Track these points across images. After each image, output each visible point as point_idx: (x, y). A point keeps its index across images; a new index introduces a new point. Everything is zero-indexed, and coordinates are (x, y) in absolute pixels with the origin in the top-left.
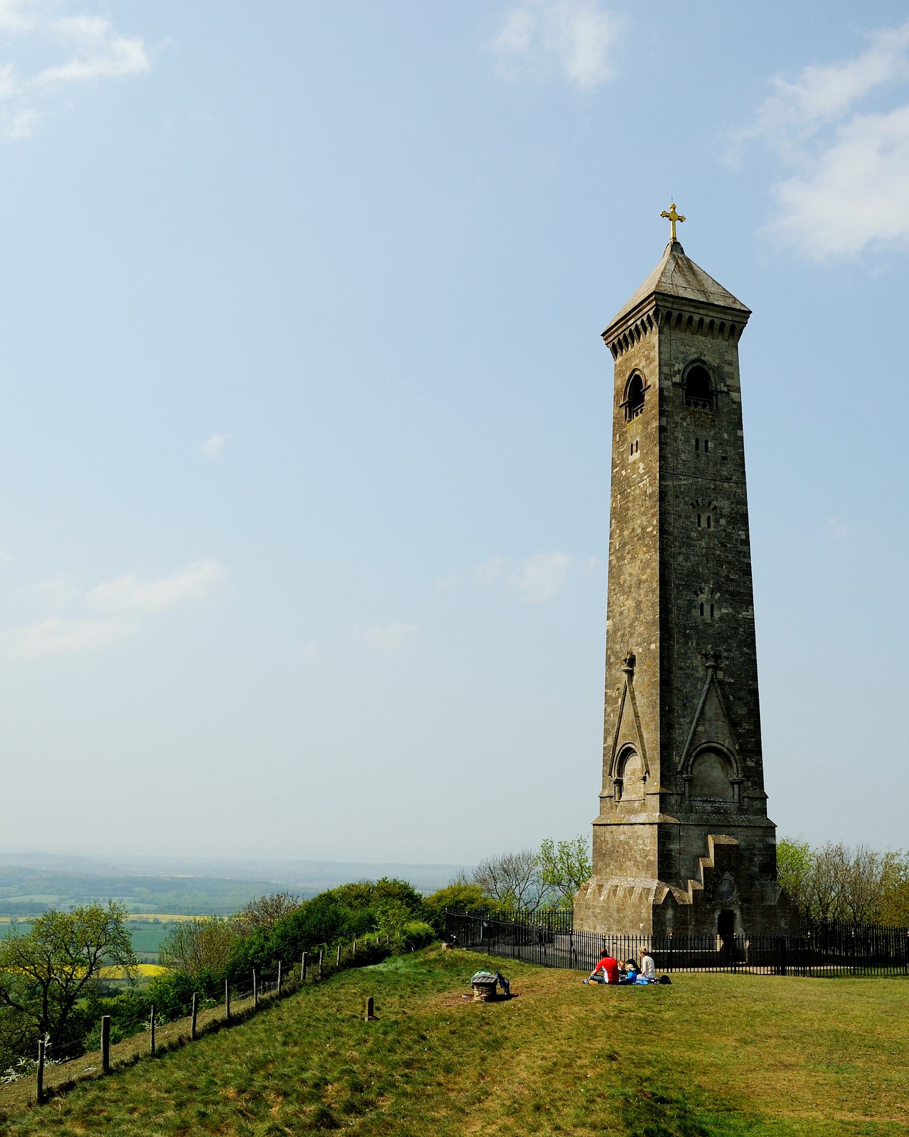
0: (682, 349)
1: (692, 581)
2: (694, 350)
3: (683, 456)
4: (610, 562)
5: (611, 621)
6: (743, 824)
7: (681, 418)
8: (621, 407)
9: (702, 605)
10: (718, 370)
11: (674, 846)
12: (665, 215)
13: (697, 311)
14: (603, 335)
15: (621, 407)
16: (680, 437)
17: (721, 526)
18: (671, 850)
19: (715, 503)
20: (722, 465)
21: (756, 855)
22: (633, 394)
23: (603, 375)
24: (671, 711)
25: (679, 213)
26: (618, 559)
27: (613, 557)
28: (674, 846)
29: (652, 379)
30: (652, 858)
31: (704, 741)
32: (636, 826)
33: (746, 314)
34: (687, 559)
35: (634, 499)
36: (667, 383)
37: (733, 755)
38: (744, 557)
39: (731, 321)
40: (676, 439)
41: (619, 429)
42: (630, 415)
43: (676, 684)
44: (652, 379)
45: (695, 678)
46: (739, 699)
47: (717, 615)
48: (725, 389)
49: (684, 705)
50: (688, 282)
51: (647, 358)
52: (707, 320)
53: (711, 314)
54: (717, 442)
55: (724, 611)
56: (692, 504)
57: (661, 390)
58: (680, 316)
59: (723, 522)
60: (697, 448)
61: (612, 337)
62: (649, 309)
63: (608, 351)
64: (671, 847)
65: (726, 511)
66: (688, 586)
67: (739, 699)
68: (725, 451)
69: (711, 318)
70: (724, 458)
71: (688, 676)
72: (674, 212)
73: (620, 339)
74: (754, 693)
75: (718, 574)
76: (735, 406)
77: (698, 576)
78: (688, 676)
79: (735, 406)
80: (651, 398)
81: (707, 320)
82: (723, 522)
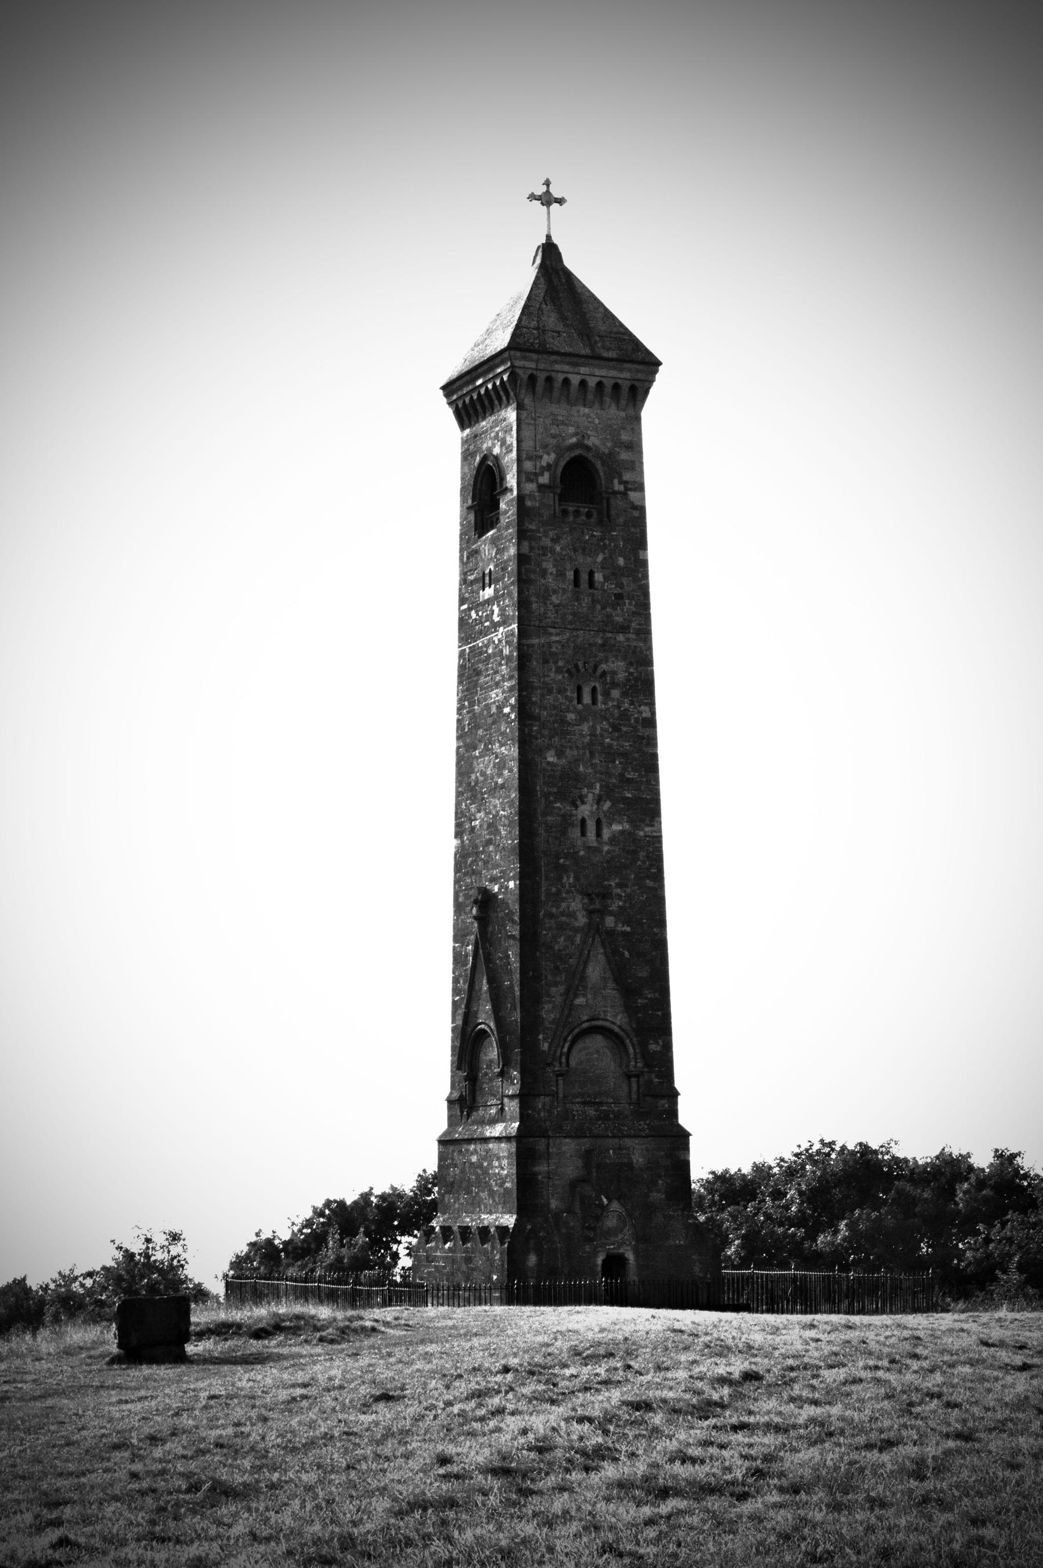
1: (568, 787)
2: (571, 430)
3: (555, 599)
9: (583, 821)
11: (542, 1168)
25: (556, 193)
33: (658, 363)
34: (560, 754)
37: (628, 1036)
39: (636, 367)
40: (544, 573)
47: (606, 834)
48: (622, 488)
50: (563, 318)
52: (592, 382)
53: (597, 372)
55: (616, 827)
58: (549, 380)
60: (576, 582)
65: (621, 676)
66: (561, 796)
68: (620, 585)
69: (598, 379)
70: (619, 597)
71: (561, 927)
76: (636, 514)
77: (577, 778)
78: (561, 927)
79: (636, 514)
81: (592, 382)
82: (615, 693)
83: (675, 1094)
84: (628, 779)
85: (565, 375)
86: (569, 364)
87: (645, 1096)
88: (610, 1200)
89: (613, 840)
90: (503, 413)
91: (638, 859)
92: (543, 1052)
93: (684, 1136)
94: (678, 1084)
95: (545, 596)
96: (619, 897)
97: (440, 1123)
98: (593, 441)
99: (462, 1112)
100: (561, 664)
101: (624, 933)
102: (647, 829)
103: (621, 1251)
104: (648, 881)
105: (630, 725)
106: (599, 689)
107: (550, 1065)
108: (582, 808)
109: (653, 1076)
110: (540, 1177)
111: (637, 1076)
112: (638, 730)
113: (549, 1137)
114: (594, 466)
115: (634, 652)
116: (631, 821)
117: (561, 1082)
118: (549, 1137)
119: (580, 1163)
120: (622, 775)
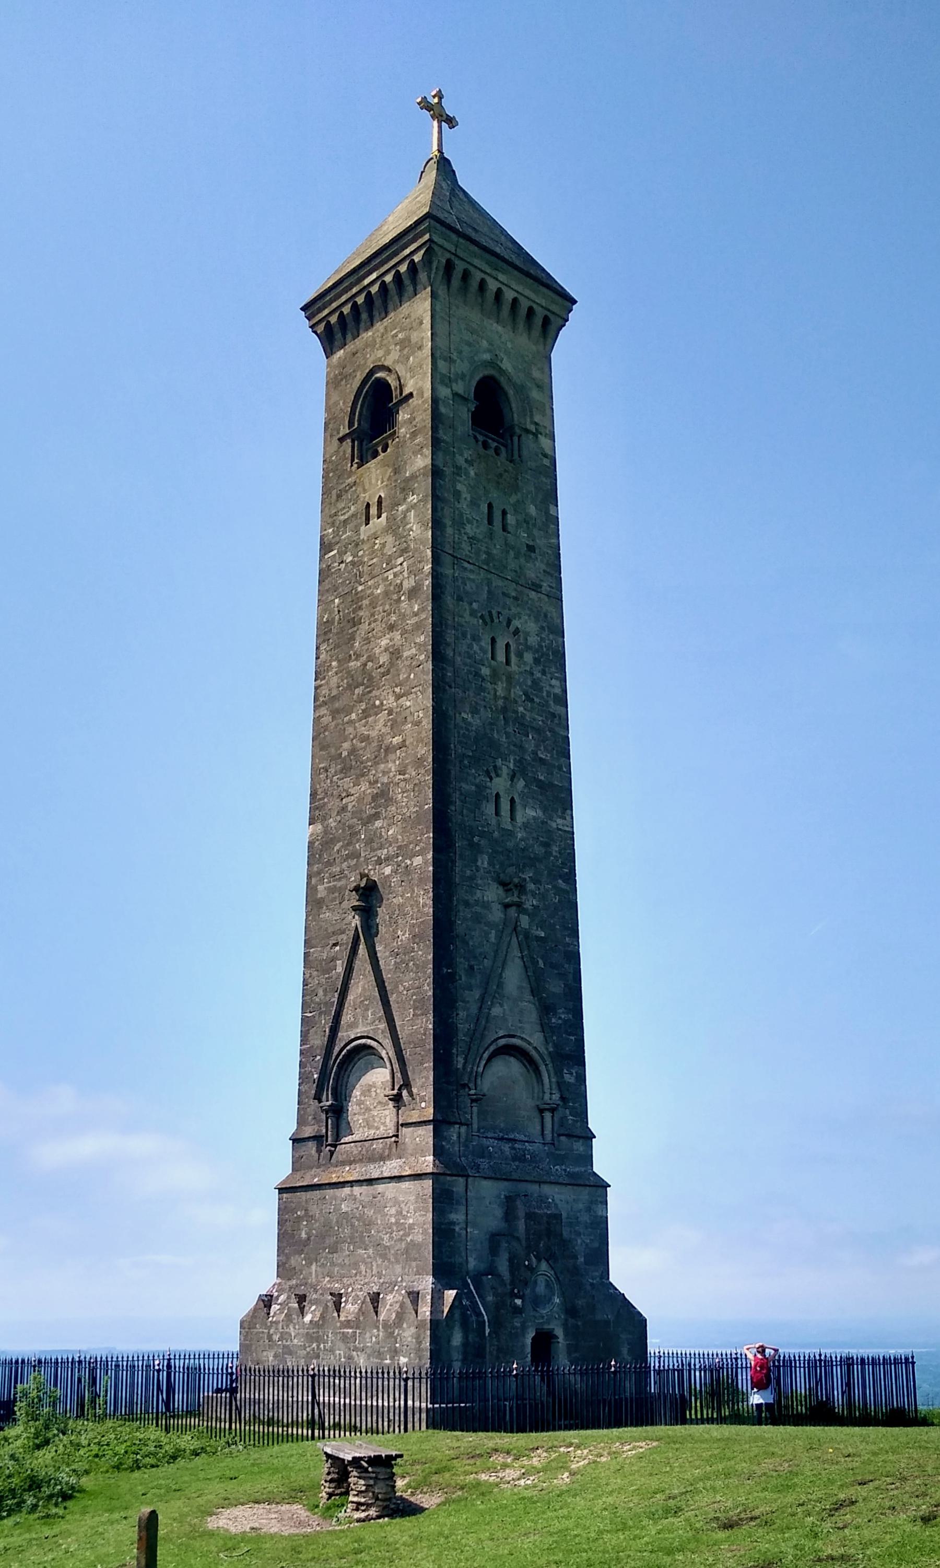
0: (467, 336)
1: (485, 752)
4: (317, 720)
5: (319, 827)
6: (561, 1180)
7: (466, 461)
8: (341, 440)
9: (498, 796)
10: (521, 389)
11: (457, 1217)
12: (425, 105)
13: (494, 273)
14: (303, 309)
15: (341, 440)
16: (466, 495)
17: (525, 663)
18: (453, 1223)
19: (516, 623)
20: (528, 558)
21: (579, 1234)
22: (370, 416)
23: (303, 385)
24: (452, 977)
26: (335, 713)
27: (323, 711)
28: (457, 1217)
29: (416, 380)
30: (419, 1238)
31: (501, 1033)
32: (380, 1188)
35: (373, 605)
36: (444, 392)
37: (544, 1061)
38: (559, 725)
39: (542, 307)
40: (457, 494)
41: (334, 489)
42: (364, 455)
43: (460, 927)
44: (416, 380)
45: (488, 924)
46: (553, 966)
47: (520, 819)
49: (471, 968)
51: (405, 344)
52: (509, 295)
54: (520, 518)
55: (531, 813)
56: (482, 617)
57: (435, 401)
59: (528, 657)
61: (326, 312)
62: (415, 252)
63: (315, 343)
64: (453, 1217)
65: (533, 640)
67: (553, 966)
69: (516, 295)
72: (440, 103)
73: (339, 316)
74: (574, 958)
75: (521, 747)
76: (546, 462)
77: (493, 744)
79: (546, 462)
80: (413, 419)
81: (509, 295)
83: (589, 1137)
84: (541, 759)
85: (483, 276)
86: (488, 263)
87: (559, 1135)
88: (539, 1260)
89: (526, 826)
90: (405, 308)
91: (551, 854)
92: (458, 1069)
93: (603, 1186)
94: (593, 1124)
95: (459, 524)
96: (534, 895)
97: (280, 1164)
98: (506, 365)
99: (319, 1151)
100: (475, 605)
101: (538, 938)
102: (559, 821)
103: (551, 1327)
104: (560, 881)
105: (542, 697)
106: (513, 647)
107: (465, 1086)
108: (496, 780)
109: (567, 1112)
110: (457, 1229)
111: (553, 1110)
112: (548, 706)
113: (468, 1176)
114: (506, 394)
115: (546, 616)
116: (545, 810)
117: (475, 1109)
118: (468, 1176)
119: (499, 1212)
120: (535, 753)
